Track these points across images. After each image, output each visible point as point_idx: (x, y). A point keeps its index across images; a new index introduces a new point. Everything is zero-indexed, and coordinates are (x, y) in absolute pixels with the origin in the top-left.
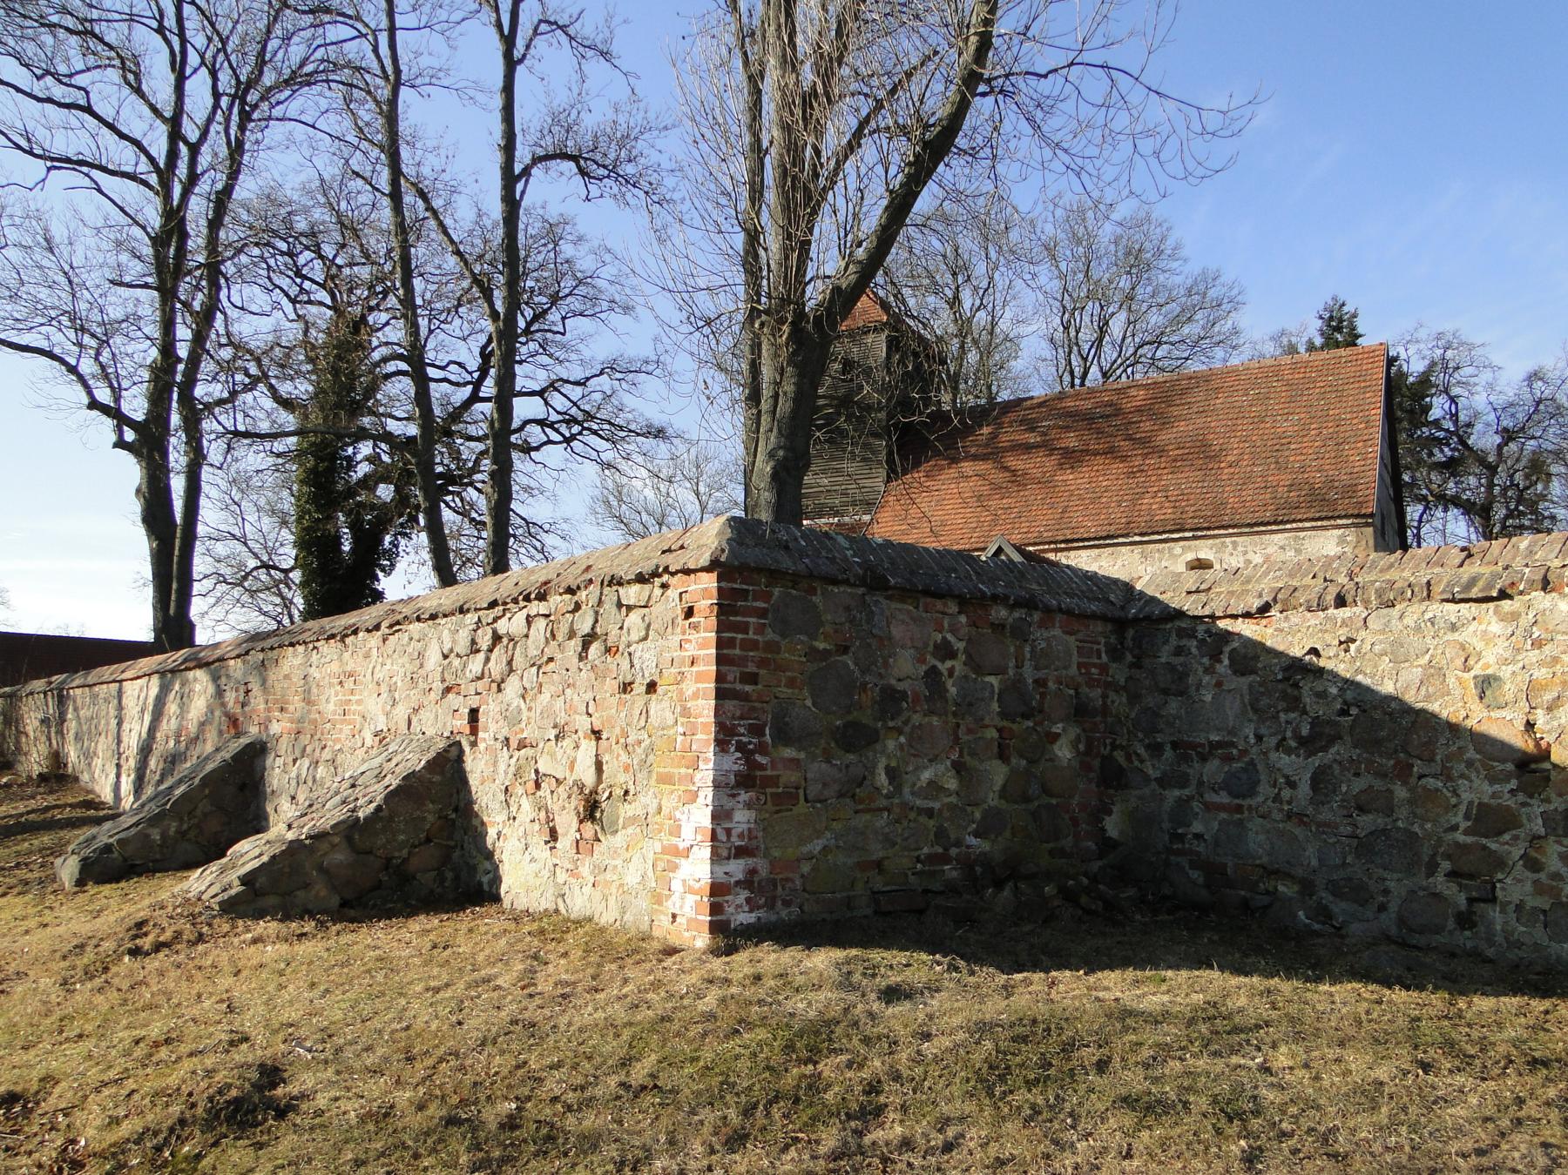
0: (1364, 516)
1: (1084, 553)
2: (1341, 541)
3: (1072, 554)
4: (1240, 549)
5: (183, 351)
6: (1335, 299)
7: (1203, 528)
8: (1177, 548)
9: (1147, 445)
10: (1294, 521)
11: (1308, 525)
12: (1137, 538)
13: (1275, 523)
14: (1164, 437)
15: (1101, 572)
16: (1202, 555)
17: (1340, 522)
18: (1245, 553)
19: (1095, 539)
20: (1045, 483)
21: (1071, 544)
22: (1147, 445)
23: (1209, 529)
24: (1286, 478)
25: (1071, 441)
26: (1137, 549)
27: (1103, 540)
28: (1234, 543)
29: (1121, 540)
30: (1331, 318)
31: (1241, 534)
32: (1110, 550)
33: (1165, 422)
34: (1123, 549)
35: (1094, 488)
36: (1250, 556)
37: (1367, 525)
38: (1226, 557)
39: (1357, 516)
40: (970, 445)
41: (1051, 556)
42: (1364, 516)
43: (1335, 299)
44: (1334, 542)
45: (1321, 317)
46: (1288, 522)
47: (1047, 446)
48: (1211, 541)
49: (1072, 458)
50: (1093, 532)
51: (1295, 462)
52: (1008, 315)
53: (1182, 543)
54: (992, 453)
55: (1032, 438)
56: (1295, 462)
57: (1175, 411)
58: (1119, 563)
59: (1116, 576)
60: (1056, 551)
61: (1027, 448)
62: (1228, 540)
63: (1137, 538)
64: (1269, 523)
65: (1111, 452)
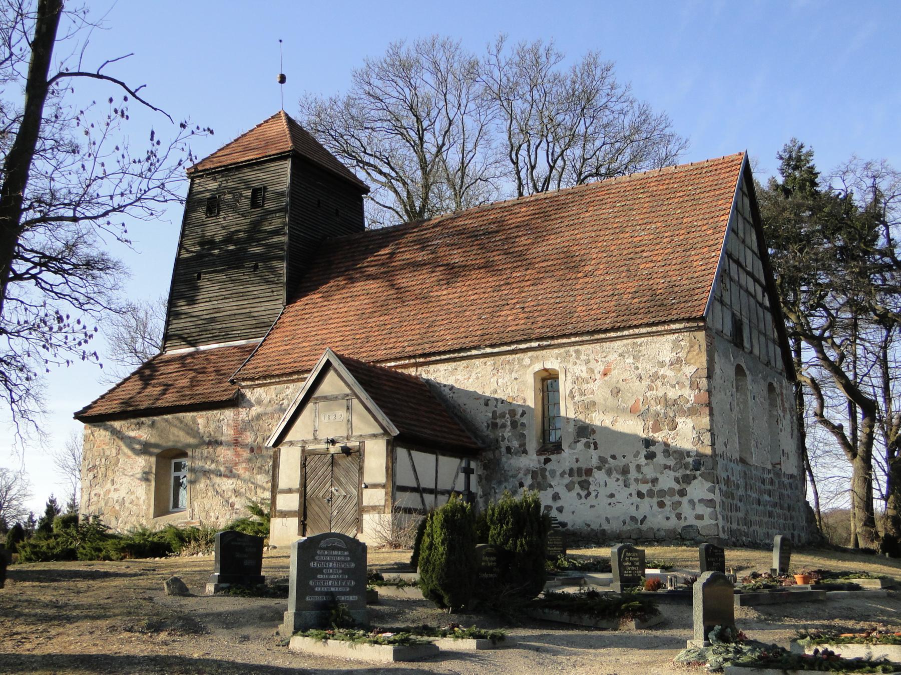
0: (695, 319)
1: (442, 367)
2: (676, 345)
3: (432, 368)
4: (583, 357)
5: (682, 326)
6: (794, 141)
7: (548, 339)
8: (526, 358)
9: (521, 259)
10: (630, 327)
11: (643, 330)
12: (488, 350)
13: (613, 329)
14: (541, 249)
15: (457, 386)
16: (548, 366)
17: (673, 326)
18: (587, 362)
19: (450, 352)
20: (424, 298)
21: (428, 357)
22: (521, 259)
23: (552, 338)
24: (632, 285)
25: (457, 258)
26: (490, 361)
27: (457, 354)
28: (577, 352)
29: (474, 352)
30: (790, 157)
31: (582, 343)
32: (464, 363)
33: (539, 235)
34: (477, 362)
35: (465, 301)
36: (592, 364)
37: (699, 329)
38: (570, 366)
39: (689, 320)
40: (370, 264)
41: (412, 372)
42: (695, 319)
43: (794, 141)
44: (669, 346)
45: (781, 158)
46: (624, 328)
47: (433, 264)
48: (556, 351)
49: (453, 273)
50: (451, 344)
51: (644, 268)
52: (478, 157)
53: (530, 354)
54: (388, 275)
55: (421, 256)
56: (644, 268)
57: (555, 224)
58: (474, 376)
59: (471, 389)
60: (417, 365)
61: (416, 266)
62: (572, 349)
63: (488, 350)
64: (606, 331)
65: (488, 266)
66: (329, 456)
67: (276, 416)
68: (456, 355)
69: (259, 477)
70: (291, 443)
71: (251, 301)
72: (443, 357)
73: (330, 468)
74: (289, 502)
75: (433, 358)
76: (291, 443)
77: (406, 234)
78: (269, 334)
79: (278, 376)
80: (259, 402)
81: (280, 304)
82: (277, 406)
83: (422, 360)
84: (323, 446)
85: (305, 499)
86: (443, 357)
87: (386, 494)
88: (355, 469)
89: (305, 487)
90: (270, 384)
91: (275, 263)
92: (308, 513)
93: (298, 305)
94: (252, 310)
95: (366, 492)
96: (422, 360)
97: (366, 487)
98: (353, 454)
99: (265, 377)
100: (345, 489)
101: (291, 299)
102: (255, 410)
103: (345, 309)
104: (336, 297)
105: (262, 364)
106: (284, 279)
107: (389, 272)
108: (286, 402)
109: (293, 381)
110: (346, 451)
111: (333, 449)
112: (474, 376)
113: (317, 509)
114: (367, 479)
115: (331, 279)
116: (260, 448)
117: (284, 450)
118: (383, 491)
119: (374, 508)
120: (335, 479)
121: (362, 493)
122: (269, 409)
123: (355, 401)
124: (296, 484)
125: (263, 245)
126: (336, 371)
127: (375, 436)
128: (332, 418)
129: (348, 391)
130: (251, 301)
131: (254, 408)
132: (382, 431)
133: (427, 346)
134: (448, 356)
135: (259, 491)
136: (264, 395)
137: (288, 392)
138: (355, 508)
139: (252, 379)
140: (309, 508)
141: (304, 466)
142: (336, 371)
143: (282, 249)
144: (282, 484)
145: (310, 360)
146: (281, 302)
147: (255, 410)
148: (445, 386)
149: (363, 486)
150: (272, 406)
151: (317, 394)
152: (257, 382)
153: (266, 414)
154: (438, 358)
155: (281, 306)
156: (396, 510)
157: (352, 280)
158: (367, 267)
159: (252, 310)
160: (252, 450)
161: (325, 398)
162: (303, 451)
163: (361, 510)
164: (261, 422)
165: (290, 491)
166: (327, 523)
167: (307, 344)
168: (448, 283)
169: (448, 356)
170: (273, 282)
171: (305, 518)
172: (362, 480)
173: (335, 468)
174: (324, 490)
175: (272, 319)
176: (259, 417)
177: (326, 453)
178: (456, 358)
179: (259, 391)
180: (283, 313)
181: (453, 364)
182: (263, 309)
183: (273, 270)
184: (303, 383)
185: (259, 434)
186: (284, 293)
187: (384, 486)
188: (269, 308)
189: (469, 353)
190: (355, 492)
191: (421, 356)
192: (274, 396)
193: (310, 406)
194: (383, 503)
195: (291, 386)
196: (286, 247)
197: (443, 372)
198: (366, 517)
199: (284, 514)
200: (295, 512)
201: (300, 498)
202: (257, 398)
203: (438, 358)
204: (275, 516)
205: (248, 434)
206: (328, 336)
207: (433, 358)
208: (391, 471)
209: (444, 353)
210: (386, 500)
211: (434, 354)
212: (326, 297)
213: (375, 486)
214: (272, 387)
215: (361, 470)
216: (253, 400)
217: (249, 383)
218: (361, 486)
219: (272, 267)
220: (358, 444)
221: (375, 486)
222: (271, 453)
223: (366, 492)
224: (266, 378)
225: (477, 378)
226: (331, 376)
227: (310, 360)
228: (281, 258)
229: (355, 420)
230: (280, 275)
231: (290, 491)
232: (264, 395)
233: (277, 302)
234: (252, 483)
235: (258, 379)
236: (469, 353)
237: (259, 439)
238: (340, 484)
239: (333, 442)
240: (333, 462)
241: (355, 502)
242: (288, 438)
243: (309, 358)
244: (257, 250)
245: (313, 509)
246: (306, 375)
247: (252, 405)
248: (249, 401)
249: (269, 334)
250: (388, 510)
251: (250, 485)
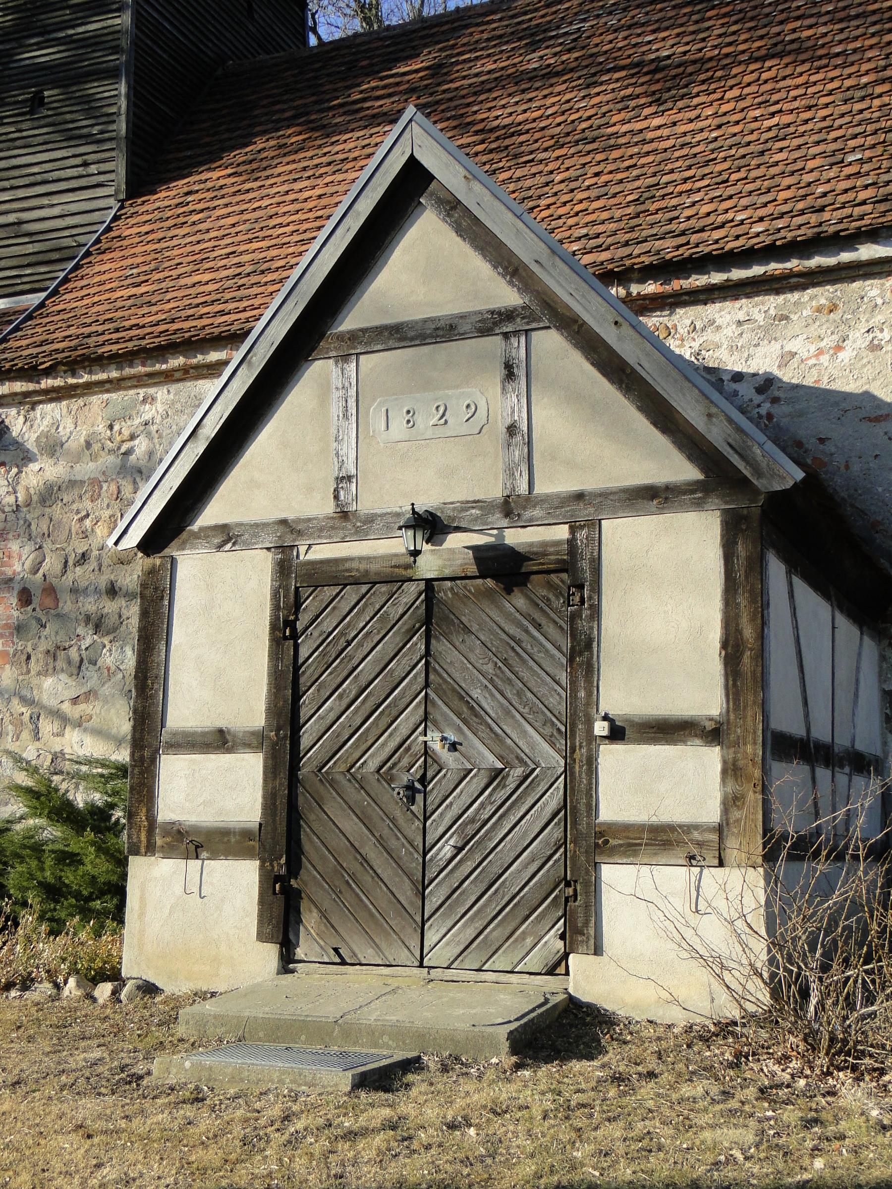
1: (725, 314)
3: (683, 317)
15: (788, 376)
19: (771, 252)
32: (822, 294)
58: (858, 339)
66: (412, 589)
67: (108, 489)
68: (793, 264)
69: (48, 682)
70: (227, 536)
71: (21, 193)
72: (737, 274)
73: (418, 643)
74: (215, 789)
75: (698, 281)
76: (227, 536)
77: (466, 27)
78: (66, 280)
79: (117, 359)
80: (53, 447)
81: (107, 200)
82: (111, 459)
83: (651, 288)
84: (398, 544)
85: (293, 780)
86: (737, 274)
87: (731, 770)
88: (551, 649)
89: (295, 726)
90: (89, 388)
91: (94, 88)
92: (310, 844)
93: (165, 197)
94: (25, 216)
95: (617, 764)
96: (651, 288)
97: (617, 734)
98: (543, 584)
99: (73, 366)
100: (496, 740)
101: (140, 184)
102: (39, 473)
103: (317, 192)
104: (280, 169)
105: (59, 335)
106: (122, 126)
107: (437, 103)
108: (141, 446)
109: (168, 377)
110: (502, 567)
111: (431, 563)
112: (858, 339)
113: (350, 825)
114: (617, 696)
115: (256, 135)
116: (50, 590)
117: (191, 565)
118: (712, 758)
119: (657, 840)
120: (438, 690)
121: (591, 763)
122: (87, 469)
123: (550, 342)
124: (248, 704)
125: (59, 42)
126: (452, 207)
127: (653, 497)
128: (427, 420)
129: (509, 296)
130: (21, 193)
131: (34, 467)
132: (686, 471)
133: (669, 243)
134: (757, 270)
135: (47, 726)
136: (67, 426)
137: (148, 412)
138: (554, 832)
139: (31, 372)
140: (312, 818)
141: (285, 631)
142: (452, 207)
143: (116, 50)
144: (184, 711)
145: (222, 313)
146: (110, 191)
147: (39, 473)
148: (738, 377)
149: (601, 728)
150: (94, 458)
151: (354, 318)
152: (47, 383)
153: (73, 484)
154: (717, 278)
155: (111, 202)
156: (780, 851)
157: (328, 131)
158: (364, 100)
159: (25, 216)
160: (25, 597)
161: (397, 335)
162: (284, 568)
163: (584, 846)
164: (57, 511)
165: (220, 741)
166: (406, 893)
167: (207, 277)
168: (658, 102)
169: (757, 270)
170: (89, 139)
171: (294, 865)
172: (592, 698)
173: (440, 646)
174: (387, 744)
175: (82, 239)
176: (49, 495)
177: (395, 576)
178: (791, 274)
179: (49, 413)
180: (116, 218)
181: (772, 303)
182: (56, 211)
183: (91, 107)
184: (209, 387)
185: (47, 546)
186: (119, 167)
187: (714, 734)
188: (74, 208)
189: (846, 257)
190: (551, 758)
191: (648, 272)
192: (101, 428)
193: (319, 377)
194: (712, 814)
195: (161, 393)
196: (125, 43)
197: (731, 331)
198: (616, 878)
199: (193, 843)
200: (246, 834)
201: (270, 772)
202: (46, 435)
203: (717, 278)
204: (151, 849)
205: (14, 546)
206: (274, 252)
207: (698, 281)
208: (743, 658)
209: (746, 257)
210: (730, 803)
211: (702, 263)
212: (255, 169)
213: (667, 730)
214: (96, 400)
215: (583, 654)
216: (30, 440)
217: (19, 386)
218: (579, 732)
219: (88, 99)
220: (562, 533)
221: (667, 730)
222: (130, 578)
223: (617, 764)
224: (80, 365)
225: (874, 347)
226: (427, 233)
227: (222, 313)
228: (113, 74)
229: (551, 422)
230: (111, 119)
231: (220, 741)
232: (67, 426)
233: (100, 192)
234: (24, 700)
235: (48, 372)
236: (846, 257)
237: (51, 564)
238: (471, 714)
239: (430, 525)
240: (434, 611)
241: (553, 800)
242: (212, 514)
243: (218, 308)
244: (45, 55)
245: (336, 823)
246: (214, 356)
247: (26, 458)
248: (18, 445)
249: (66, 280)
250: (747, 843)
251: (18, 707)
